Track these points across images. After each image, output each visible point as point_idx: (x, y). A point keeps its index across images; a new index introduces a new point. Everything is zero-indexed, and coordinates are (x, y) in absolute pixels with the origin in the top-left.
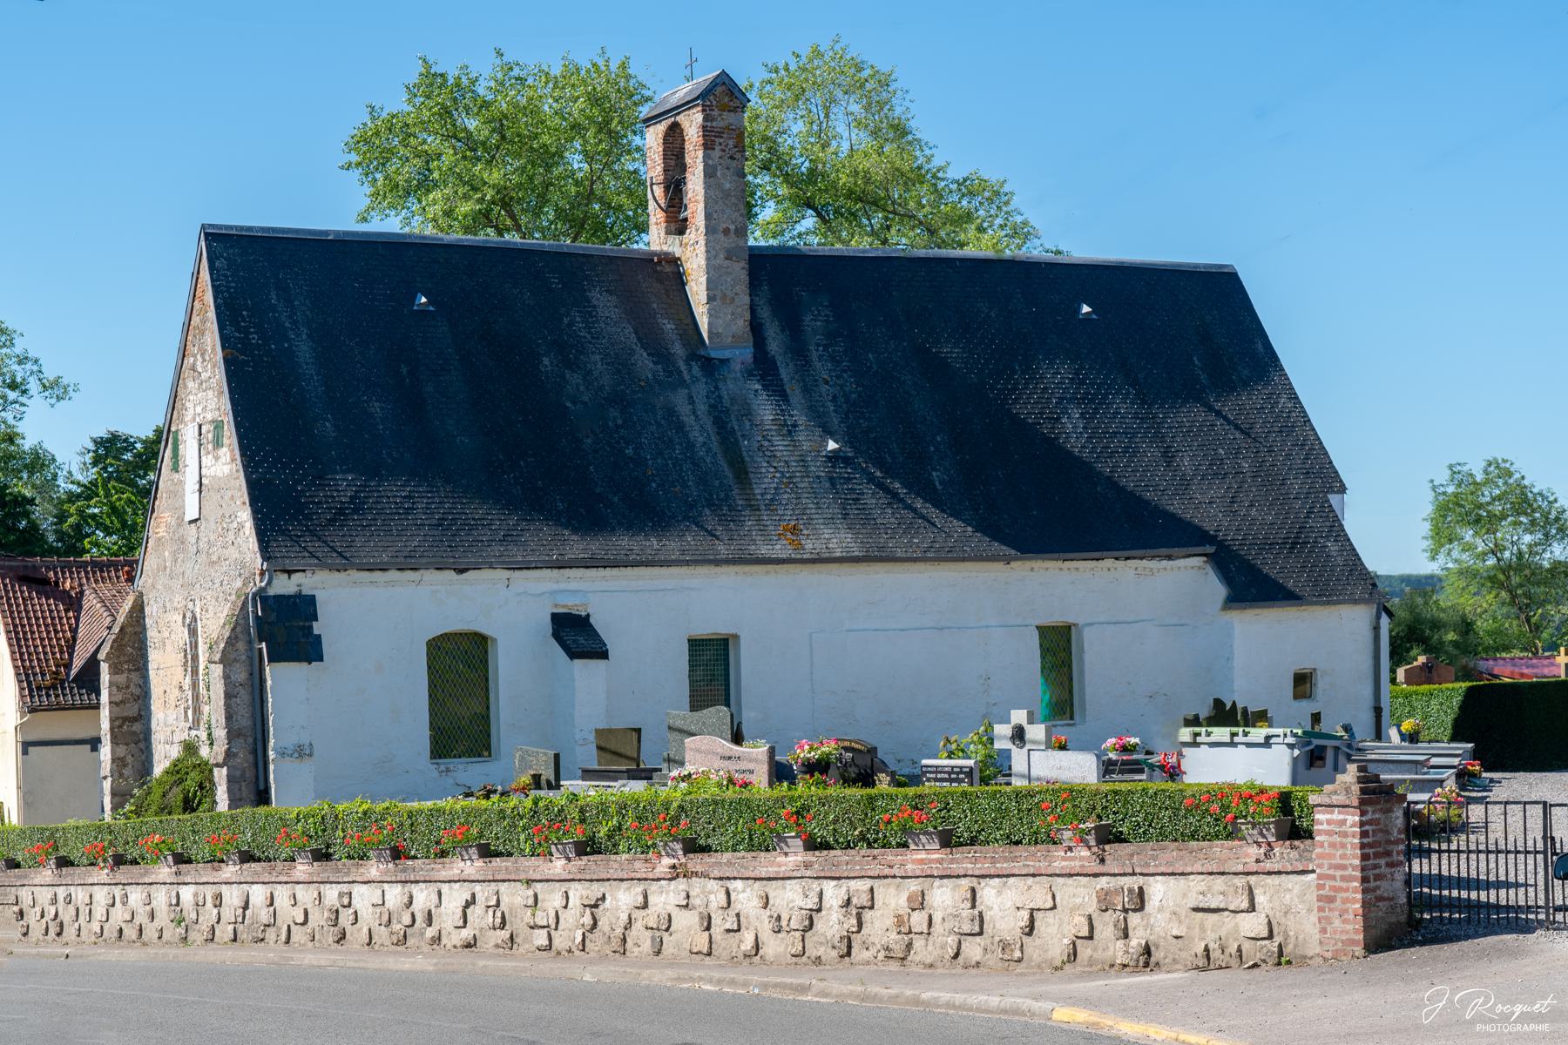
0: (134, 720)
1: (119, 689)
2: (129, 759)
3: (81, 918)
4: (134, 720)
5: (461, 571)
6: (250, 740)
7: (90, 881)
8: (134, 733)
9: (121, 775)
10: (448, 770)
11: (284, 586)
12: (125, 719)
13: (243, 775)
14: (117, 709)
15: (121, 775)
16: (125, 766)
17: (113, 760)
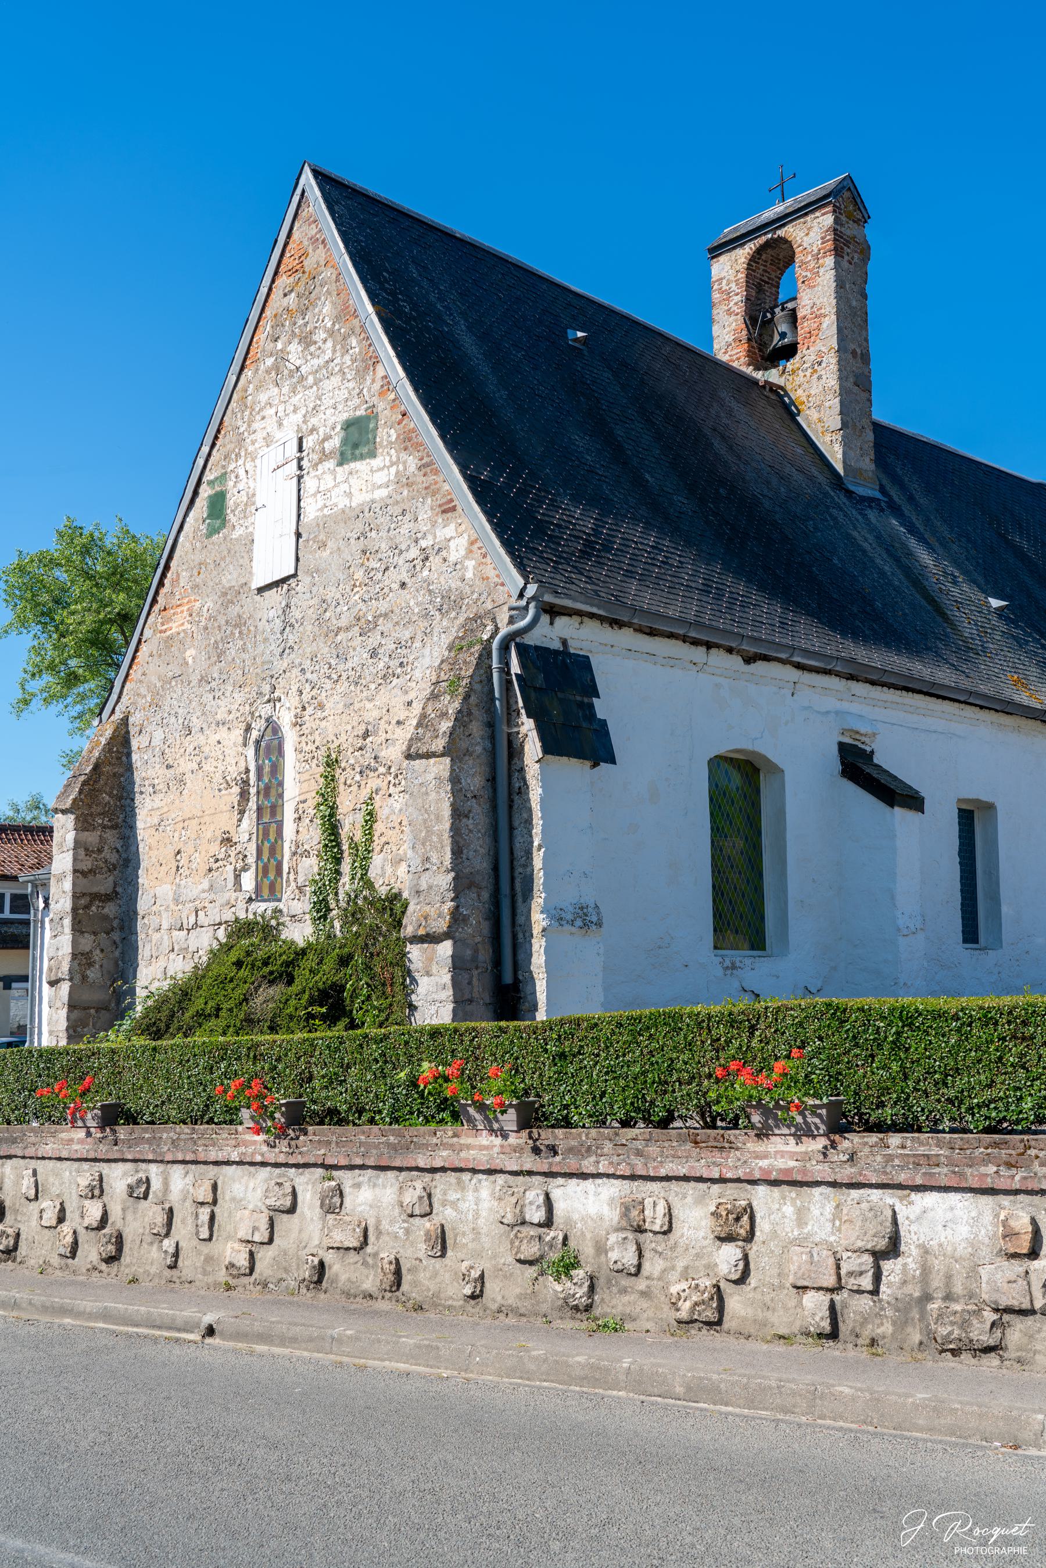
0: (107, 898)
1: (88, 852)
2: (97, 955)
3: (182, 1231)
4: (107, 898)
5: (749, 660)
6: (486, 895)
7: (213, 1155)
8: (106, 918)
9: (84, 978)
10: (733, 967)
11: (550, 634)
12: (95, 897)
13: (474, 958)
14: (83, 881)
15: (84, 978)
16: (90, 965)
17: (74, 956)
